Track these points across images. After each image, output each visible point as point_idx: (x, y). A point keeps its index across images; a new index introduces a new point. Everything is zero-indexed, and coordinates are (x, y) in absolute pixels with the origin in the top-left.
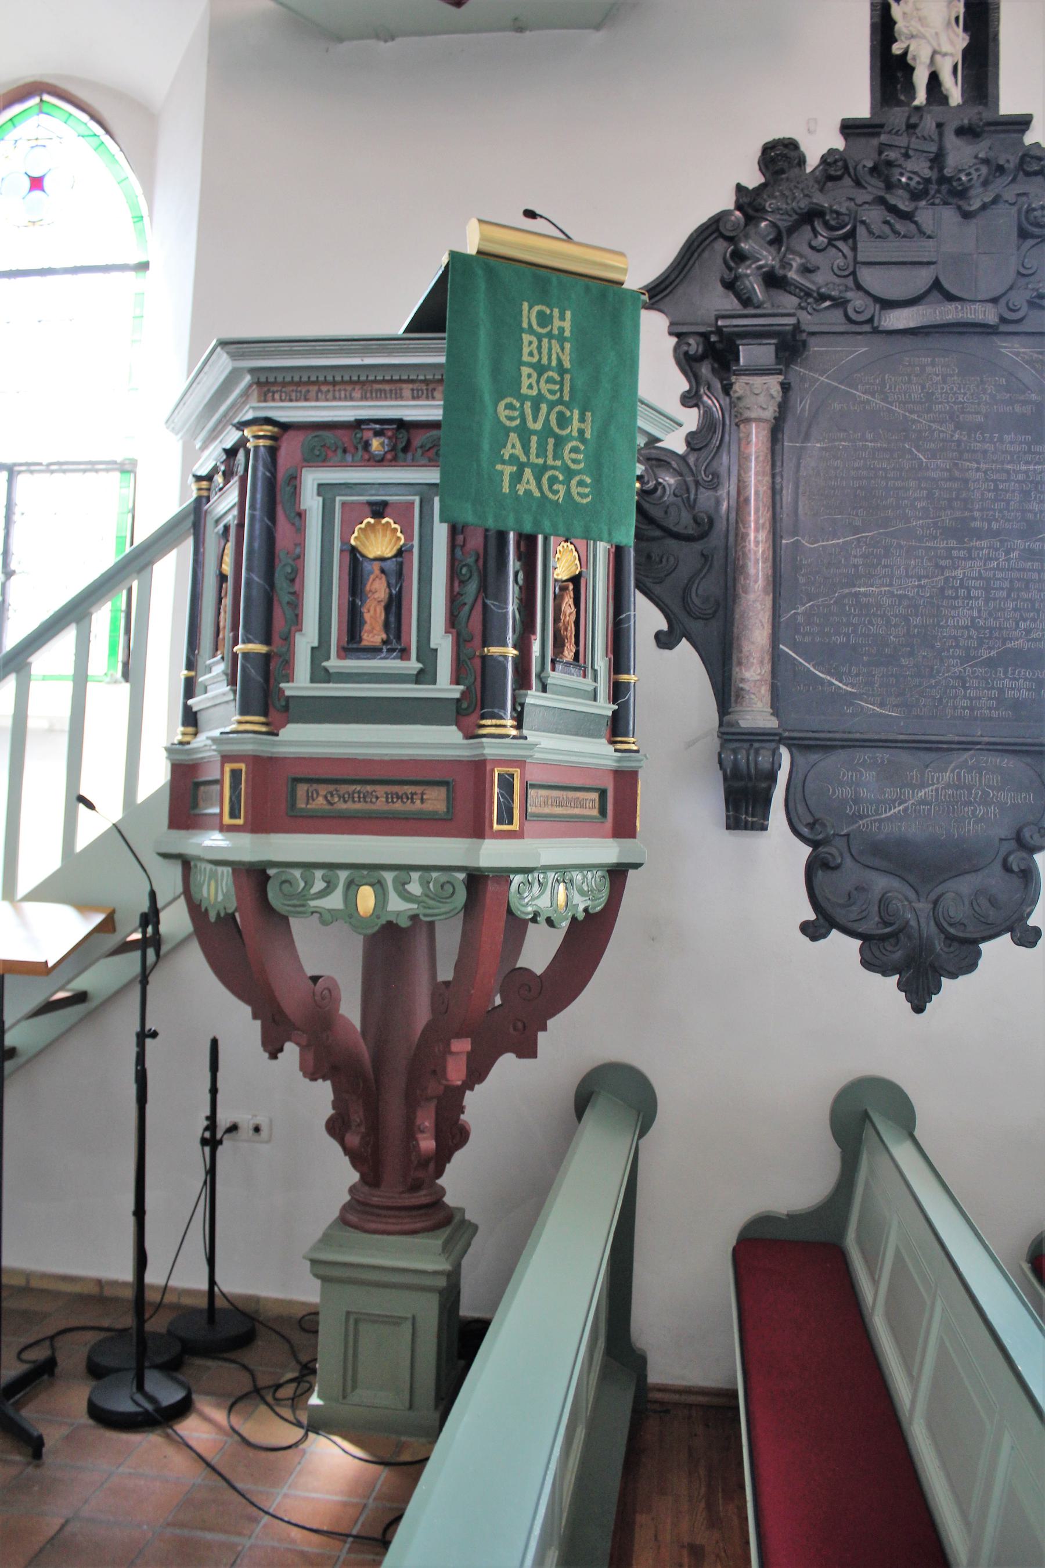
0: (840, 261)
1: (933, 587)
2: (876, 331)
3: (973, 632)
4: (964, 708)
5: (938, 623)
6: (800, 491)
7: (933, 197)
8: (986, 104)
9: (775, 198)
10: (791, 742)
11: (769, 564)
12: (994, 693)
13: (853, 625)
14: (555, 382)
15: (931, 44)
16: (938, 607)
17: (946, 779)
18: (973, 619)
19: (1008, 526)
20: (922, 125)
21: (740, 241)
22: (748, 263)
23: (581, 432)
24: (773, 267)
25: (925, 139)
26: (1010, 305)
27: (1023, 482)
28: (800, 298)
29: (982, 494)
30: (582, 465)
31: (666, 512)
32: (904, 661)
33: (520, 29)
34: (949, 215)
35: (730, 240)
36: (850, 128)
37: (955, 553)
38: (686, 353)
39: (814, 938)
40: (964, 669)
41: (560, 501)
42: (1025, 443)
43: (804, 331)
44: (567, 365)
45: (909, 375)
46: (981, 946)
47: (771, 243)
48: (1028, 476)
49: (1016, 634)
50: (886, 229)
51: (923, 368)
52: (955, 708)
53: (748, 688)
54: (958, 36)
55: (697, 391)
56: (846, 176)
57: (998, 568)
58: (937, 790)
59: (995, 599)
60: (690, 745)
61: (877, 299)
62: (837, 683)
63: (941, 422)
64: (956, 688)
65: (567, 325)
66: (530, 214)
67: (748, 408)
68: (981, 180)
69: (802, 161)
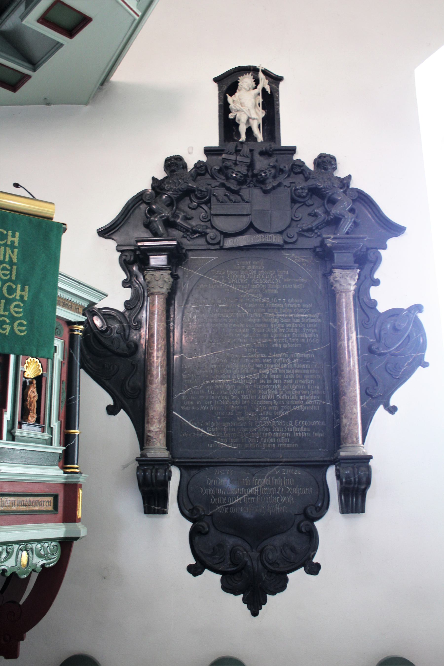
0: (203, 215)
1: (254, 379)
2: (222, 248)
3: (275, 402)
4: (272, 443)
5: (257, 398)
6: (183, 330)
7: (249, 183)
8: (275, 142)
9: (170, 183)
10: (179, 464)
11: (164, 368)
12: (288, 434)
13: (212, 400)
14: (7, 270)
15: (246, 114)
16: (257, 389)
17: (264, 482)
18: (275, 395)
19: (292, 346)
20: (243, 150)
21: (152, 204)
22: (156, 215)
23: (22, 297)
24: (168, 217)
25: (244, 156)
26: (289, 235)
27: (299, 323)
28: (183, 232)
29: (278, 330)
30: (21, 315)
31: (112, 342)
32: (239, 419)
33: (48, 104)
34: (257, 192)
35: (148, 204)
36: (208, 151)
37: (264, 361)
38: (125, 260)
39: (195, 575)
40: (272, 422)
41: (7, 334)
42: (299, 303)
43: (184, 248)
44: (15, 260)
45: (239, 270)
46: (288, 575)
47: (168, 206)
48: (301, 320)
49: (298, 402)
50: (226, 198)
51: (246, 266)
52: (267, 443)
53: (152, 436)
54: (260, 111)
55: (130, 280)
56: (207, 174)
57: (287, 368)
58: (259, 488)
59: (286, 384)
60: (125, 467)
61: (221, 233)
62: (204, 431)
63: (256, 294)
64: (267, 432)
65: (16, 240)
66: (16, 185)
67: (153, 287)
68: (272, 175)
69: (185, 166)
